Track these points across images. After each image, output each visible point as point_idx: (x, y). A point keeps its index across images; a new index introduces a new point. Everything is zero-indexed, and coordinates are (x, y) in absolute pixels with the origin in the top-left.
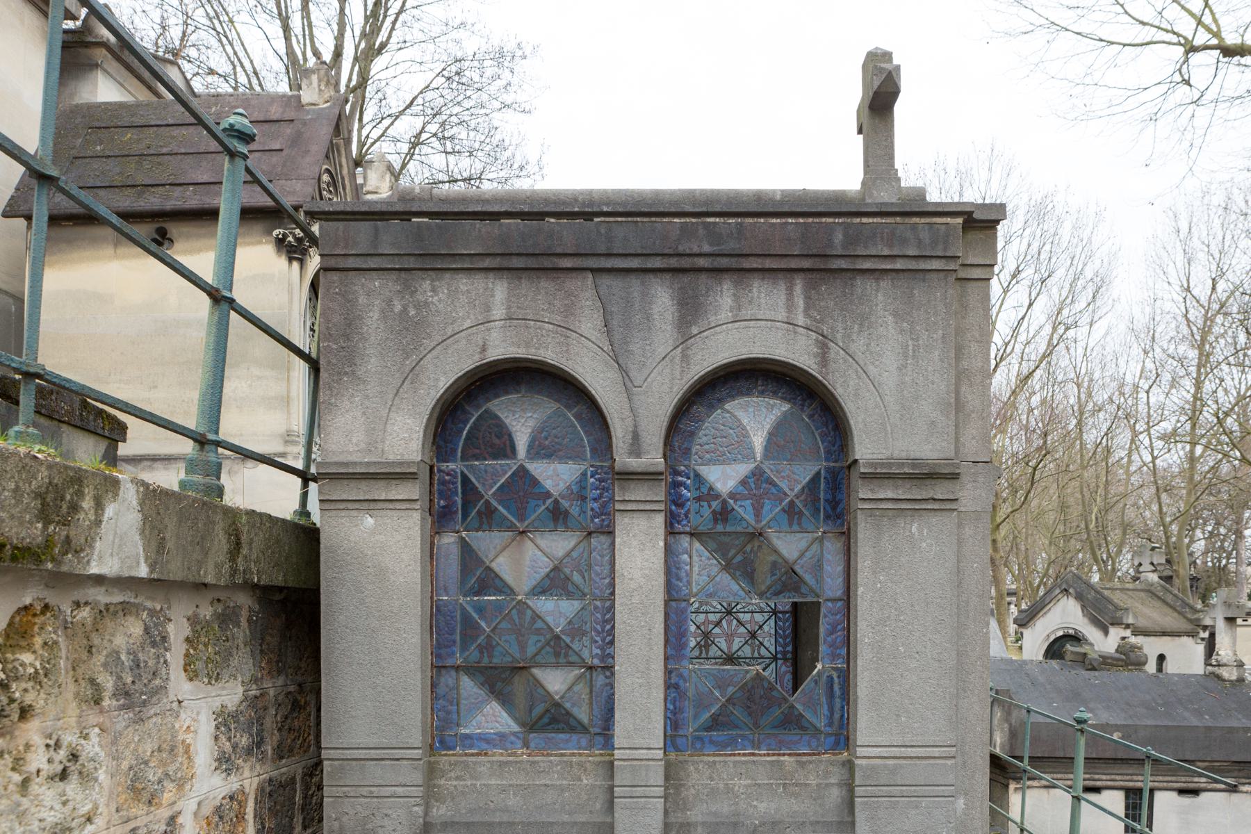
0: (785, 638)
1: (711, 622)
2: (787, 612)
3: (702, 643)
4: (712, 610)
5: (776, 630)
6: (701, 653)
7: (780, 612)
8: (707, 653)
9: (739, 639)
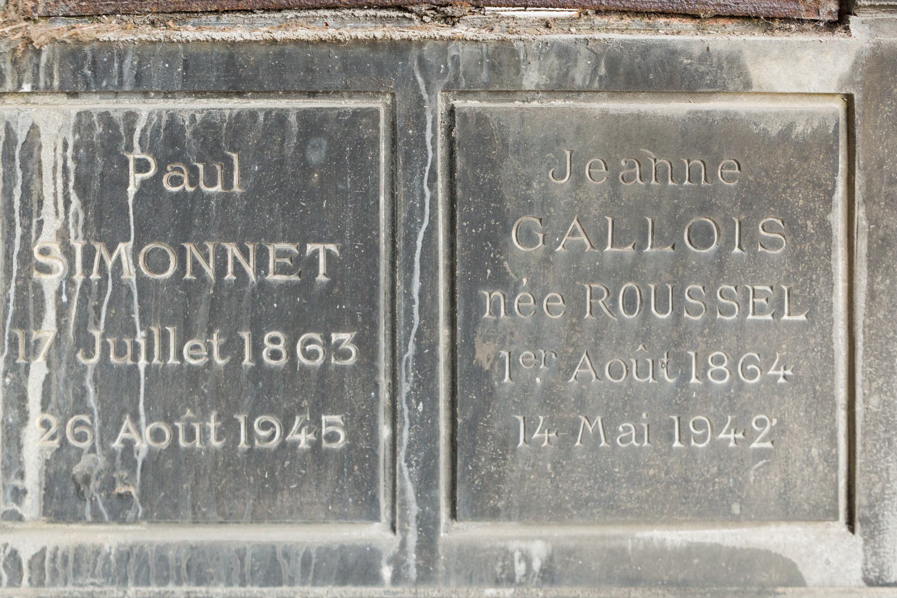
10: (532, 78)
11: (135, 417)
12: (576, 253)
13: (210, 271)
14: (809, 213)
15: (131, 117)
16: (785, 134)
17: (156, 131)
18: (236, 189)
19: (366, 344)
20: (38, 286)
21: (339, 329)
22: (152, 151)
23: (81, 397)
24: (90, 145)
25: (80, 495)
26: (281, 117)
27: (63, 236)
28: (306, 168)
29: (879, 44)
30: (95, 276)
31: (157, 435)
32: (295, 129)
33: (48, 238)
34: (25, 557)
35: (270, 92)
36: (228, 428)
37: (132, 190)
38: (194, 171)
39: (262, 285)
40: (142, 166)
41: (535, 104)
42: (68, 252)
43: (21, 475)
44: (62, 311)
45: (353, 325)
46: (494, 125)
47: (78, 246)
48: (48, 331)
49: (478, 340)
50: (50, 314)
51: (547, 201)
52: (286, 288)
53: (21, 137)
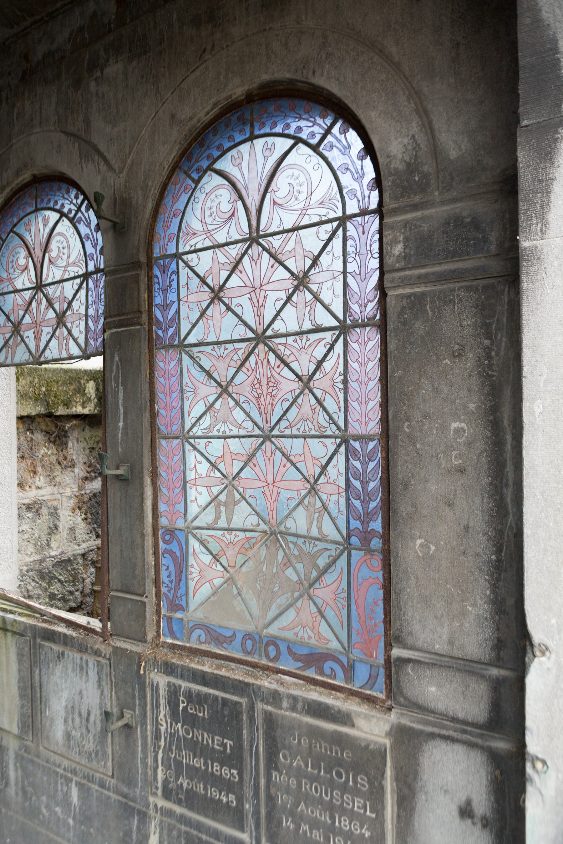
0: (366, 498)
1: (234, 456)
2: (370, 438)
3: (222, 497)
4: (235, 432)
5: (348, 481)
6: (218, 518)
7: (357, 438)
8: (229, 520)
9: (289, 494)
10: (285, 704)
11: (183, 777)
12: (299, 767)
13: (200, 738)
14: (376, 778)
15: (180, 686)
16: (367, 747)
17: (186, 692)
18: (206, 716)
19: (240, 774)
20: (160, 729)
21: (234, 769)
22: (185, 698)
23: (170, 765)
24: (171, 692)
25: (171, 794)
26: (216, 697)
27: (165, 716)
28: (224, 716)
29: (400, 723)
30: (173, 731)
31: (188, 784)
32: (220, 702)
33: (161, 716)
34: (159, 806)
35: (425, 265)
36: (205, 789)
37: (181, 708)
38: (195, 708)
39: (213, 748)
40: (183, 702)
41: (288, 713)
42: (167, 722)
43: (157, 782)
44: (165, 739)
45: (236, 769)
46: (274, 717)
47: (169, 721)
48: (162, 743)
49: (271, 786)
50: (163, 739)
51: (290, 748)
52: (219, 750)
53: (155, 685)
